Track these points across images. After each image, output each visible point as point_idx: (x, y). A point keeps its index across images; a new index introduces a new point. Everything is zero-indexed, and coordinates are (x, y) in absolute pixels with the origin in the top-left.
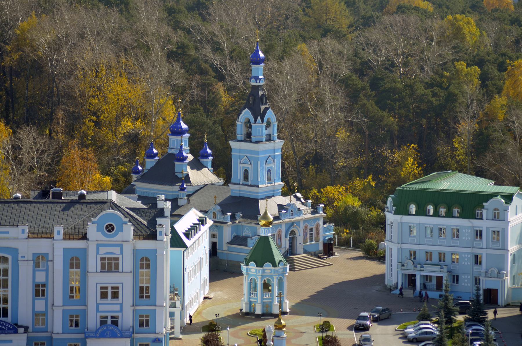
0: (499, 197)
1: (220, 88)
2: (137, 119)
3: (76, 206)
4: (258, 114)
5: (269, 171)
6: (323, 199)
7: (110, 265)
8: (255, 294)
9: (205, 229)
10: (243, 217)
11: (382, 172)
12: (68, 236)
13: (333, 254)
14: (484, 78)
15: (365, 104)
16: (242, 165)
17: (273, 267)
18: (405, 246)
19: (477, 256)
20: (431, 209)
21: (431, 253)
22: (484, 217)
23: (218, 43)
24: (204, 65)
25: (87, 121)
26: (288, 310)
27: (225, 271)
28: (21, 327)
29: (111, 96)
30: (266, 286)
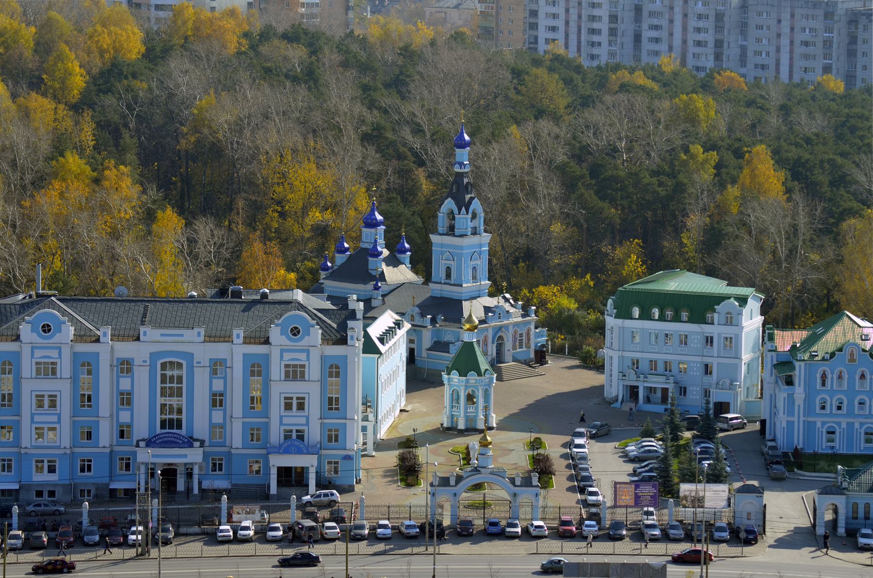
0: (732, 299)
1: (421, 174)
4: (463, 205)
5: (474, 268)
6: (535, 300)
7: (295, 372)
9: (401, 333)
10: (444, 320)
12: (249, 340)
13: (546, 363)
15: (583, 194)
18: (626, 354)
19: (707, 366)
20: (656, 312)
21: (666, 362)
22: (716, 322)
24: (402, 149)
26: (495, 425)
28: (197, 440)
30: (470, 398)
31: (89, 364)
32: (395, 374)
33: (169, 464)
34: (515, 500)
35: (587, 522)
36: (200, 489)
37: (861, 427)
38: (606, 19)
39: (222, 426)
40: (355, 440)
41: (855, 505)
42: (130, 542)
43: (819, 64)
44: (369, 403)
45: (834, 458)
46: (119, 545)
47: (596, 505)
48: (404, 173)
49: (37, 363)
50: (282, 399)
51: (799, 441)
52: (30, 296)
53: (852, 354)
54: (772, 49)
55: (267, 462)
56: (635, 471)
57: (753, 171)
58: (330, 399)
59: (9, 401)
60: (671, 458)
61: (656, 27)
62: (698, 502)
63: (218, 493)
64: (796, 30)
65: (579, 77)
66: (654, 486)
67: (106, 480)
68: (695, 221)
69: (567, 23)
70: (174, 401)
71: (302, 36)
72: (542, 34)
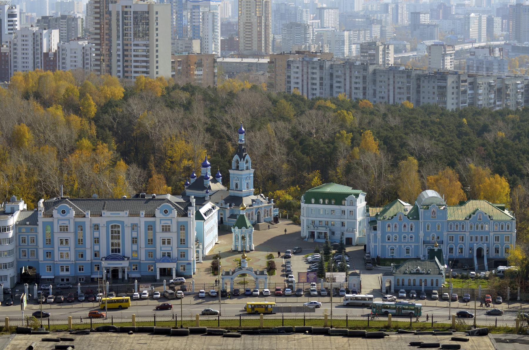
0: (353, 195)
1: (229, 144)
2: (190, 160)
3: (151, 201)
4: (242, 157)
5: (247, 184)
6: (275, 196)
7: (166, 229)
9: (215, 211)
10: (235, 205)
11: (304, 183)
12: (147, 216)
13: (279, 222)
14: (353, 139)
15: (295, 152)
16: (235, 181)
18: (310, 218)
19: (343, 223)
20: (321, 200)
21: (328, 222)
22: (346, 204)
23: (229, 124)
24: (222, 134)
25: (167, 161)
26: (254, 249)
27: (227, 231)
28: (126, 257)
29: (177, 149)
30: (243, 238)
31: (81, 226)
32: (211, 229)
33: (115, 267)
34: (257, 281)
35: (287, 289)
36: (128, 277)
37: (404, 247)
38: (318, 79)
39: (137, 252)
40: (192, 256)
41: (398, 280)
42: (97, 300)
43: (405, 96)
44: (199, 240)
45: (393, 260)
46: (92, 301)
47: (292, 282)
48: (221, 145)
49: (60, 226)
50: (161, 240)
51: (379, 254)
52: (58, 199)
53: (400, 217)
54: (386, 90)
55: (155, 266)
56: (310, 267)
57: (366, 141)
58: (79, 240)
59: (82, 242)
60: (324, 261)
61: (339, 82)
62: (334, 280)
63: (134, 279)
64: (395, 82)
65: (303, 103)
66: (315, 274)
67: (90, 274)
68: (342, 162)
69: (303, 81)
70: (116, 241)
71: (190, 88)
72: (293, 85)
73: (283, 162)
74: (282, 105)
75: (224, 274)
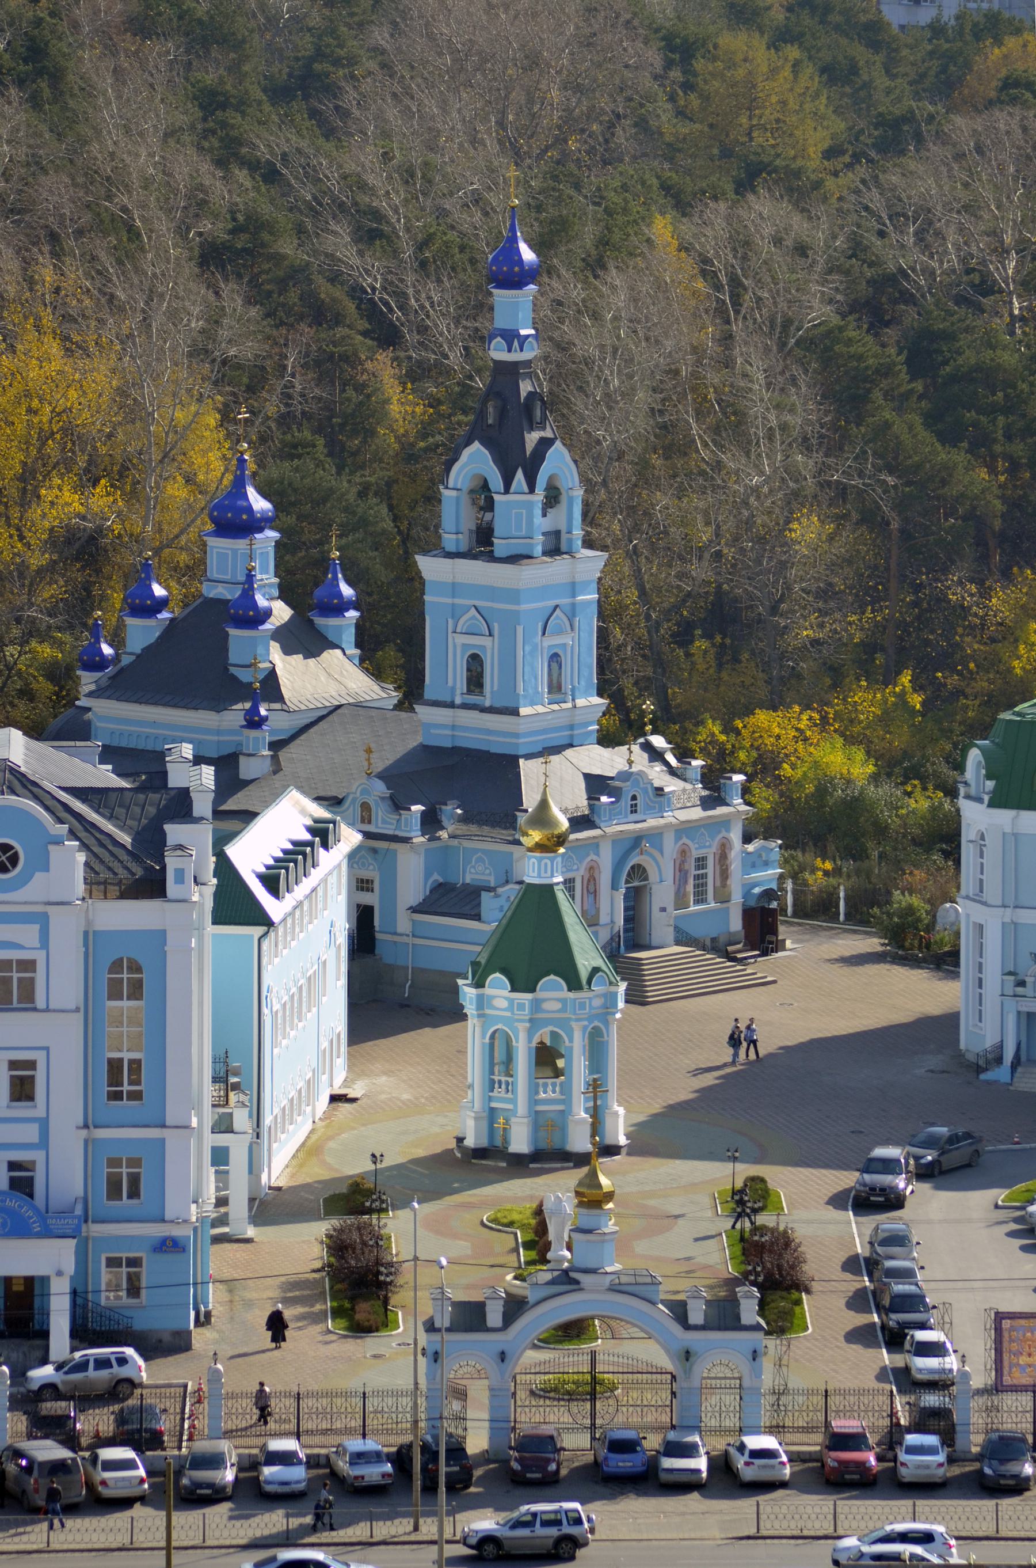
6: (742, 755)
8: (507, 1084)
10: (465, 819)
11: (948, 659)
13: (779, 946)
15: (887, 425)
17: (570, 990)
24: (325, 290)
26: (623, 1141)
27: (404, 1005)
32: (313, 984)
34: (688, 1372)
58: (115, 1067)
73: (795, 499)
74: (741, 73)
75: (444, 1321)
